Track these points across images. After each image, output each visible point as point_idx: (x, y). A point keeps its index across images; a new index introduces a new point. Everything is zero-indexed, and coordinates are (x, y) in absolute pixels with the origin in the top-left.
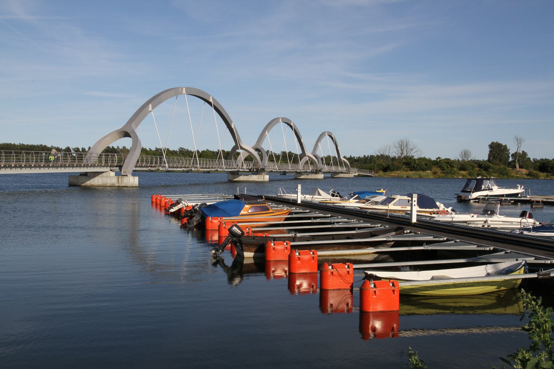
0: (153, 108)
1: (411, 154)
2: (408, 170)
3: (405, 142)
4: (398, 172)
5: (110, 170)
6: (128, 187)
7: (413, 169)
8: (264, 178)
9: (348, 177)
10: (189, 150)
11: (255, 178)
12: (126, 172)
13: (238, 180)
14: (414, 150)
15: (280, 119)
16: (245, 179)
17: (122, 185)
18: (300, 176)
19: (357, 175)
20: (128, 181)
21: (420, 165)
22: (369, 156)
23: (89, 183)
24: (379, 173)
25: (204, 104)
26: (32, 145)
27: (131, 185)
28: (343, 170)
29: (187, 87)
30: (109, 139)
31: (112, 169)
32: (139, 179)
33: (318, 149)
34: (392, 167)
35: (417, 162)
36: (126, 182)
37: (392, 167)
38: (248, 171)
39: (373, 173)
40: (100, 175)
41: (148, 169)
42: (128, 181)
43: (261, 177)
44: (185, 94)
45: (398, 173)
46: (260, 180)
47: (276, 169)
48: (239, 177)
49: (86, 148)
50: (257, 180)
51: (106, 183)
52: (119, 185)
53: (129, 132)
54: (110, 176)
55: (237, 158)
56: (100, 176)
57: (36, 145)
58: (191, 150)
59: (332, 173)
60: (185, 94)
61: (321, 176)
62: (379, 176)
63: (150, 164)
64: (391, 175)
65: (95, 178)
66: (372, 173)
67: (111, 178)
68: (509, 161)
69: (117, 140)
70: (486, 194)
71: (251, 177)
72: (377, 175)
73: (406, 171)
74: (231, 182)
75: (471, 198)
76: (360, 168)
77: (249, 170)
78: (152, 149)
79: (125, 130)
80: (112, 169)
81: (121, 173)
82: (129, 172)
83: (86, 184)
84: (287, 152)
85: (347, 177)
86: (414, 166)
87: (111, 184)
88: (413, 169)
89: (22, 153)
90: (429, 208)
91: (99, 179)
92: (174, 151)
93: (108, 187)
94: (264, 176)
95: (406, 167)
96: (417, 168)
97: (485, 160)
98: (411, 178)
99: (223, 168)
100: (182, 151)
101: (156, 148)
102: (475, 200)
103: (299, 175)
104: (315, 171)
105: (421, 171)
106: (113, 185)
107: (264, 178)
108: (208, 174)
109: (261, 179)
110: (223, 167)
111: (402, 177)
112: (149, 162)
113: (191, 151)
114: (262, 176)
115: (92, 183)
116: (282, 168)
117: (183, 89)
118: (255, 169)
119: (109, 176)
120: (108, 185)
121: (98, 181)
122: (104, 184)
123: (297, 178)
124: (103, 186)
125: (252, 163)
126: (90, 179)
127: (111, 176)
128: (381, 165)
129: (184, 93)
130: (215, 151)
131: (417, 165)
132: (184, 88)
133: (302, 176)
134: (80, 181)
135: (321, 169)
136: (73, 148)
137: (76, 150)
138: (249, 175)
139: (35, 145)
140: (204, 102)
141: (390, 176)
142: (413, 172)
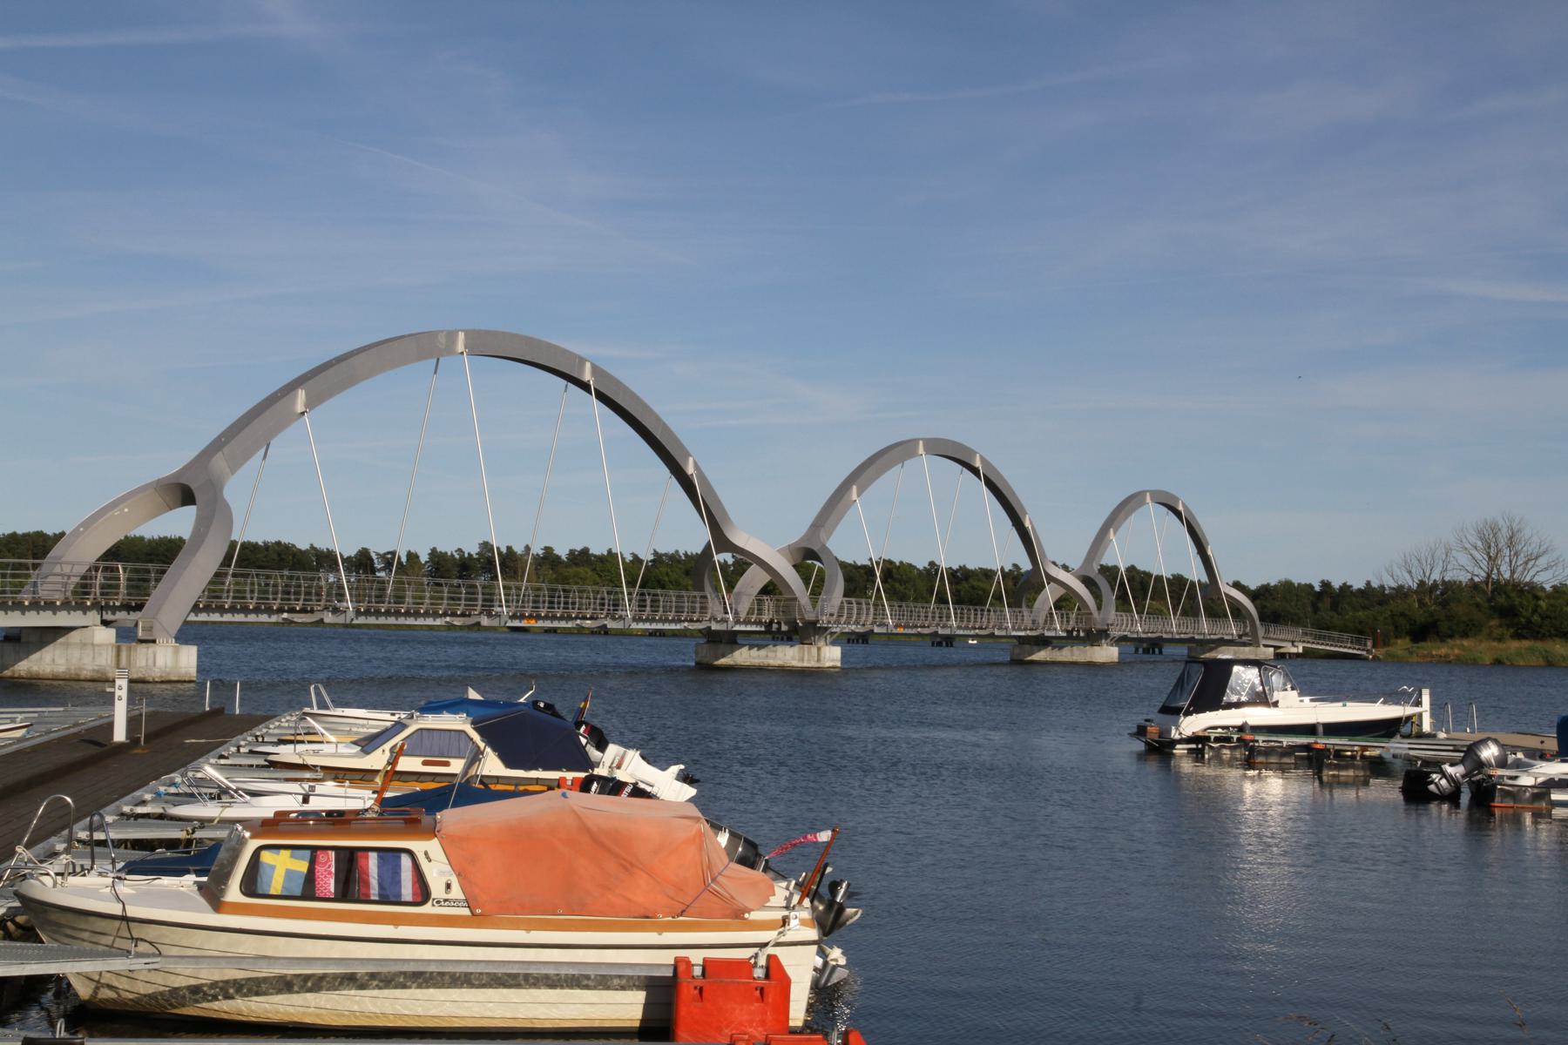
0: (311, 404)
1: (1532, 573)
3: (1504, 530)
4: (1466, 643)
5: (99, 621)
6: (149, 682)
7: (1525, 631)
8: (819, 655)
11: (787, 655)
12: (152, 627)
13: (732, 663)
14: (1542, 562)
16: (754, 658)
18: (1032, 654)
19: (1301, 650)
21: (1555, 618)
22: (424, 558)
24: (1396, 644)
25: (566, 391)
26: (166, 538)
27: (161, 677)
29: (474, 331)
30: (126, 510)
31: (108, 616)
32: (199, 657)
36: (143, 663)
38: (763, 629)
39: (1369, 644)
41: (574, 626)
43: (809, 652)
44: (462, 353)
45: (1463, 648)
46: (805, 664)
48: (732, 652)
49: (419, 554)
50: (796, 663)
54: (93, 644)
55: (737, 581)
57: (260, 543)
59: (1194, 645)
60: (462, 353)
61: (1107, 653)
62: (1389, 655)
63: (676, 612)
64: (1434, 653)
65: (44, 650)
67: (96, 649)
69: (157, 516)
70: (1239, 722)
71: (776, 651)
72: (1380, 652)
73: (1500, 639)
74: (706, 667)
75: (1177, 737)
76: (1323, 628)
77: (765, 627)
79: (183, 481)
80: (108, 616)
82: (165, 630)
83: (13, 672)
84: (1155, 574)
86: (1529, 621)
87: (94, 670)
88: (1525, 630)
90: (546, 768)
91: (57, 653)
93: (86, 680)
95: (1500, 626)
96: (1540, 627)
98: (1512, 664)
101: (656, 553)
102: (1194, 746)
104: (1082, 634)
105: (1558, 640)
106: (102, 673)
107: (819, 655)
109: (809, 661)
110: (345, 604)
111: (1474, 663)
112: (674, 609)
114: (814, 650)
115: (35, 668)
117: (457, 336)
118: (785, 623)
120: (85, 674)
121: (53, 660)
122: (73, 672)
123: (1021, 657)
124: (67, 677)
128: (1403, 614)
129: (460, 351)
130: (859, 564)
131: (1543, 618)
136: (378, 554)
137: (388, 559)
138: (767, 646)
139: (257, 543)
141: (1433, 656)
142: (1526, 643)
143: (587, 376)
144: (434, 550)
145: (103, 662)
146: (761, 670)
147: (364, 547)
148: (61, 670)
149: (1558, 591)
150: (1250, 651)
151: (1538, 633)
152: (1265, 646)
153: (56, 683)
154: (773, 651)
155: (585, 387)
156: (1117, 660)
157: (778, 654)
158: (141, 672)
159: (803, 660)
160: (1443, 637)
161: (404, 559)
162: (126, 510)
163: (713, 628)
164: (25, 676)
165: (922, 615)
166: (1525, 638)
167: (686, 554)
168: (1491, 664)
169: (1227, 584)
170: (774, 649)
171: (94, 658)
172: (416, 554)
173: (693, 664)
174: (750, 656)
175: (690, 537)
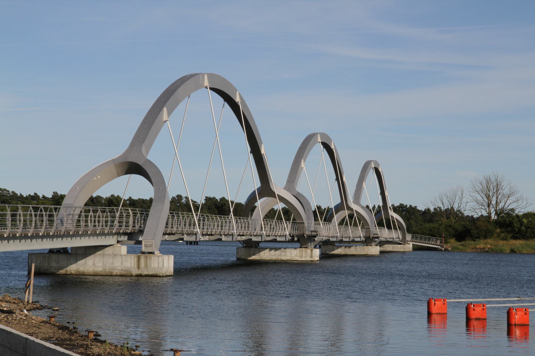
1: (507, 204)
2: (509, 238)
4: (489, 241)
6: (160, 276)
7: (518, 235)
8: (311, 254)
9: (402, 250)
10: (16, 194)
13: (259, 258)
15: (319, 135)
16: (272, 256)
17: (146, 273)
18: (334, 250)
20: (161, 265)
23: (73, 268)
28: (226, 230)
33: (364, 192)
34: (476, 231)
35: (525, 221)
36: (156, 266)
37: (474, 232)
40: (98, 253)
42: (161, 265)
43: (306, 252)
46: (303, 259)
47: (360, 237)
51: (112, 269)
52: (139, 272)
53: (140, 163)
54: (121, 255)
56: (99, 255)
57: (137, 199)
58: (22, 194)
65: (88, 258)
66: (437, 242)
67: (123, 257)
68: (408, 207)
71: (285, 252)
78: (16, 192)
81: (141, 247)
83: (66, 271)
85: (399, 250)
86: (520, 230)
87: (122, 270)
88: (518, 235)
89: (106, 211)
92: (39, 196)
94: (312, 250)
95: (502, 232)
97: (25, 196)
99: (196, 234)
100: (3, 195)
103: (330, 247)
106: (128, 271)
107: (311, 254)
108: (196, 247)
109: (305, 257)
111: (501, 252)
113: (21, 194)
114: (309, 251)
115: (82, 269)
116: (175, 229)
119: (120, 254)
122: (107, 271)
124: (104, 274)
125: (290, 222)
126: (76, 261)
127: (122, 254)
128: (450, 226)
131: (526, 228)
132: (206, 75)
133: (338, 248)
134: (54, 264)
135: (313, 234)
140: (222, 100)
145: (129, 265)
146: (275, 263)
147: (214, 196)
148: (99, 270)
149: (527, 215)
150: (401, 247)
151: (525, 236)
153: (97, 278)
154: (284, 252)
157: (287, 253)
158: (155, 270)
159: (302, 257)
160: (474, 238)
162: (99, 177)
163: (331, 240)
164: (74, 273)
166: (518, 239)
168: (510, 252)
170: (285, 250)
171: (122, 263)
173: (236, 259)
174: (270, 255)
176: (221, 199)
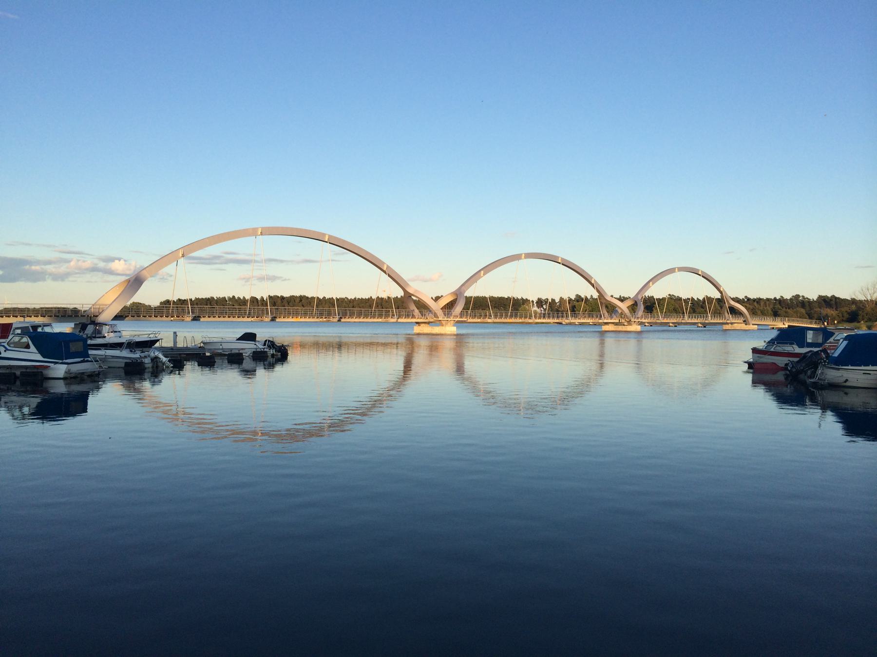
143: (700, 273)
144: (552, 299)
152: (753, 324)
155: (700, 275)
156: (70, 344)
161: (550, 301)
165: (682, 316)
167: (648, 296)
169: (432, 298)
172: (767, 298)
175: (399, 293)
176: (832, 296)
